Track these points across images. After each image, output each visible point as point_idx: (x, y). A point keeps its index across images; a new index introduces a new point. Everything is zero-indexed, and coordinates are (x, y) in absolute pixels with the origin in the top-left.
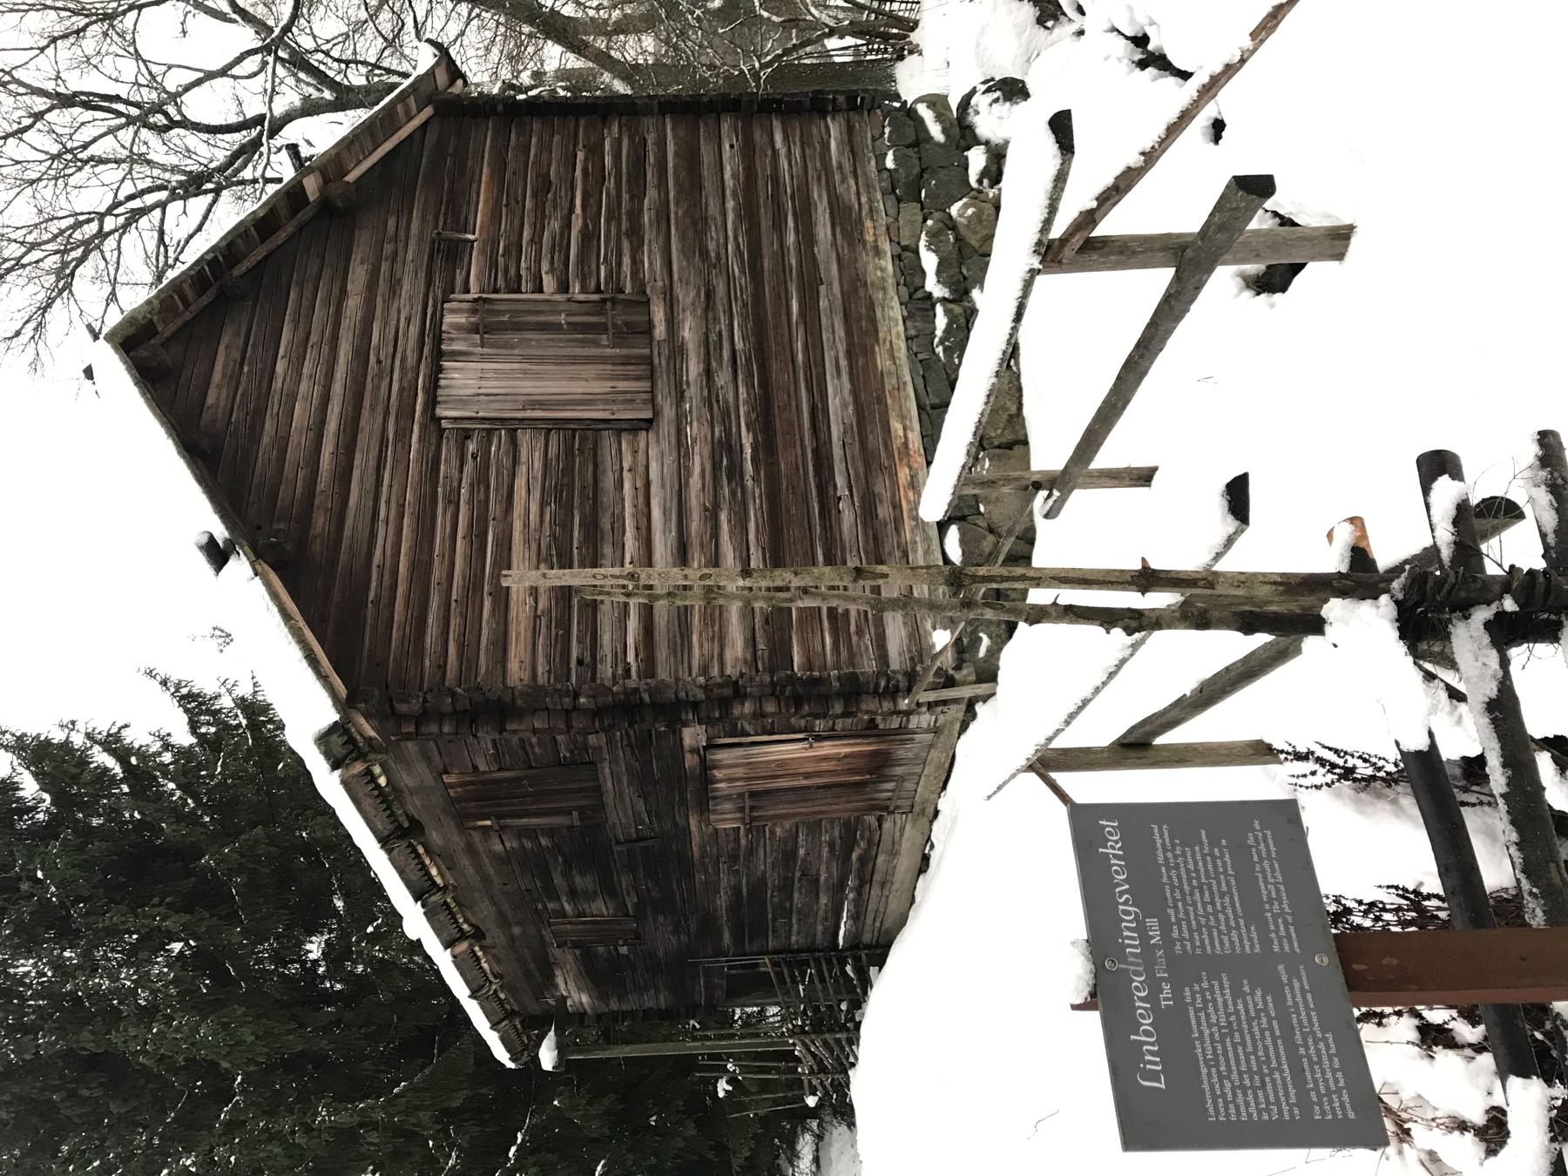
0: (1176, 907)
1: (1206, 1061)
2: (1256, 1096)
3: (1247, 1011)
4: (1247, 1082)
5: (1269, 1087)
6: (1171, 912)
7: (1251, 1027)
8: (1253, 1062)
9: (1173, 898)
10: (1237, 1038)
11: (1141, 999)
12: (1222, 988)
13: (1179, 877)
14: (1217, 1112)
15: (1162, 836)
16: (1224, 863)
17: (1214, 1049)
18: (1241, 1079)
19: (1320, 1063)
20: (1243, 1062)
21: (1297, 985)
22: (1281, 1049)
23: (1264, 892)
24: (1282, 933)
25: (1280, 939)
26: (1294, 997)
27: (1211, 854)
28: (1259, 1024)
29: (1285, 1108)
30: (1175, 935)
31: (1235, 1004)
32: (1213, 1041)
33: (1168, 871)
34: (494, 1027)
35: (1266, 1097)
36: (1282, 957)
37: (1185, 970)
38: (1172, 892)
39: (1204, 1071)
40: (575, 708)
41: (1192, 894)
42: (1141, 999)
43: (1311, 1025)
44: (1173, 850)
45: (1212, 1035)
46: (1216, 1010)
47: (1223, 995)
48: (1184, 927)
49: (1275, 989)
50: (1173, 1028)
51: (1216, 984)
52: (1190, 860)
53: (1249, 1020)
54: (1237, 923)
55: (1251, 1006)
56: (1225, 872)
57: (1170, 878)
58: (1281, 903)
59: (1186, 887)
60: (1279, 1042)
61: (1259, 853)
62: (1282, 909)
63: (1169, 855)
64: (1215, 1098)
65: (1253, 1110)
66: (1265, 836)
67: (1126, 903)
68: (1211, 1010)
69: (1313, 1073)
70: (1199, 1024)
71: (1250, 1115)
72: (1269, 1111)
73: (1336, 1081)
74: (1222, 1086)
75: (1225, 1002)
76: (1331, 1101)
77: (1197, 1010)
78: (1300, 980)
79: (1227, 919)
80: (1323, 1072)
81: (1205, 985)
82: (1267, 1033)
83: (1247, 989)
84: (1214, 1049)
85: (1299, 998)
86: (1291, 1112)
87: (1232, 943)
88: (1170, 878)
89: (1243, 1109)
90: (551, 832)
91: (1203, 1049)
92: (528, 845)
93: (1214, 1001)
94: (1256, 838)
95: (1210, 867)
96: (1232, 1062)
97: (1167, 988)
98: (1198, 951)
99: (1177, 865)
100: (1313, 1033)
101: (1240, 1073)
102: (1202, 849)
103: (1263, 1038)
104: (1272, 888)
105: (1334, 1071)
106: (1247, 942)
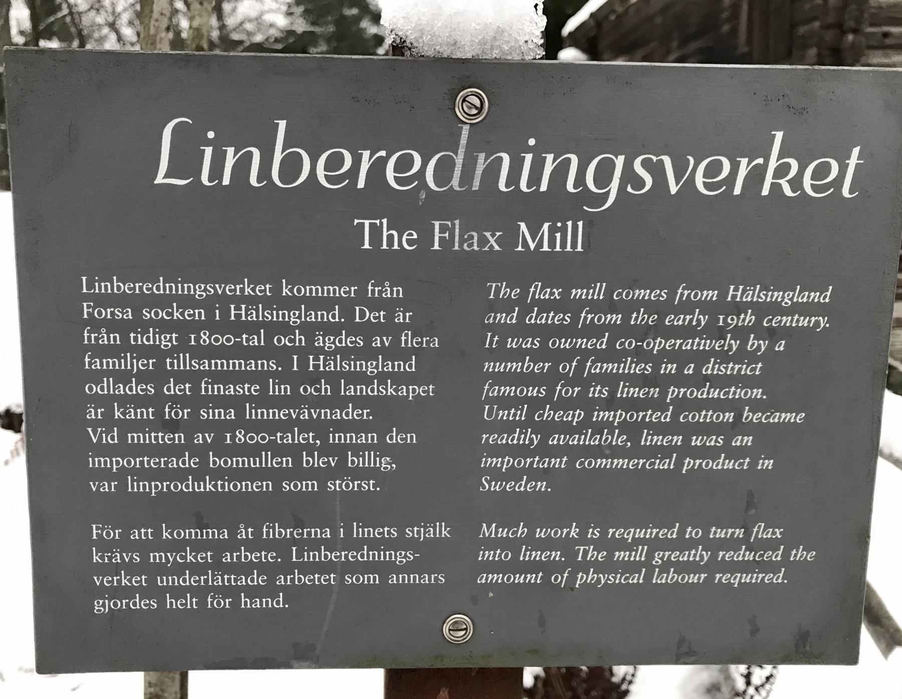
0: (610, 306)
1: (224, 301)
2: (140, 401)
3: (342, 426)
4: (172, 389)
5: (163, 438)
6: (598, 292)
7: (305, 426)
8: (218, 414)
9: (635, 305)
10: (275, 389)
11: (378, 168)
12: (399, 379)
13: (688, 332)
14: (102, 301)
15: (796, 309)
16: (711, 453)
17: (252, 328)
18: (181, 377)
19: (218, 566)
20: (218, 389)
21: (401, 557)
22: (253, 487)
23: (630, 534)
24: (526, 555)
25: (512, 545)
26: (374, 545)
27: (737, 427)
28: (310, 449)
29: (116, 463)
30: (537, 291)
31: (360, 402)
32: (274, 328)
33: (706, 307)
34: (592, 15)
35: (139, 426)
36: (467, 539)
37: (445, 291)
38: (650, 307)
39: (199, 291)
40: (844, 32)
41: (640, 355)
42: (378, 168)
43: (306, 568)
44: (757, 330)
45: (285, 329)
46: (345, 353)
47: (382, 378)
48: (554, 318)
49: (391, 504)
50: (298, 235)
51: (411, 366)
52: (732, 368)
53: (321, 428)
54: (556, 452)
55: (350, 438)
56: (687, 450)
57: (687, 307)
58: (600, 567)
59: (657, 345)
60: (267, 486)
61: (731, 544)
62: (585, 566)
63: (749, 318)
64: (138, 302)
65: (106, 387)
66: (772, 568)
67: (629, 176)
68: (346, 340)
69: (198, 546)
70: (314, 304)
71: (97, 377)
72: (108, 422)
73: (178, 592)
74: (164, 327)
75: (367, 380)
76: (132, 569)
77: (347, 306)
78: (408, 568)
79: (567, 429)
80: (198, 569)
81: (407, 339)
82: (287, 462)
83: (395, 438)
84: (252, 328)
85: (366, 555)
86: (105, 474)
87: (508, 427)
88: (687, 307)
89: (109, 363)
90: (734, 31)
91: (252, 301)
92: (725, 15)
93: (368, 353)
94: (772, 545)
95: (707, 416)
96: (219, 364)
97: (405, 241)
98: (491, 341)
99: (720, 334)
100: (287, 568)
101: (194, 377)
102: (756, 405)
103: (279, 451)
104: (640, 554)
105: (200, 592)
106: (504, 466)
